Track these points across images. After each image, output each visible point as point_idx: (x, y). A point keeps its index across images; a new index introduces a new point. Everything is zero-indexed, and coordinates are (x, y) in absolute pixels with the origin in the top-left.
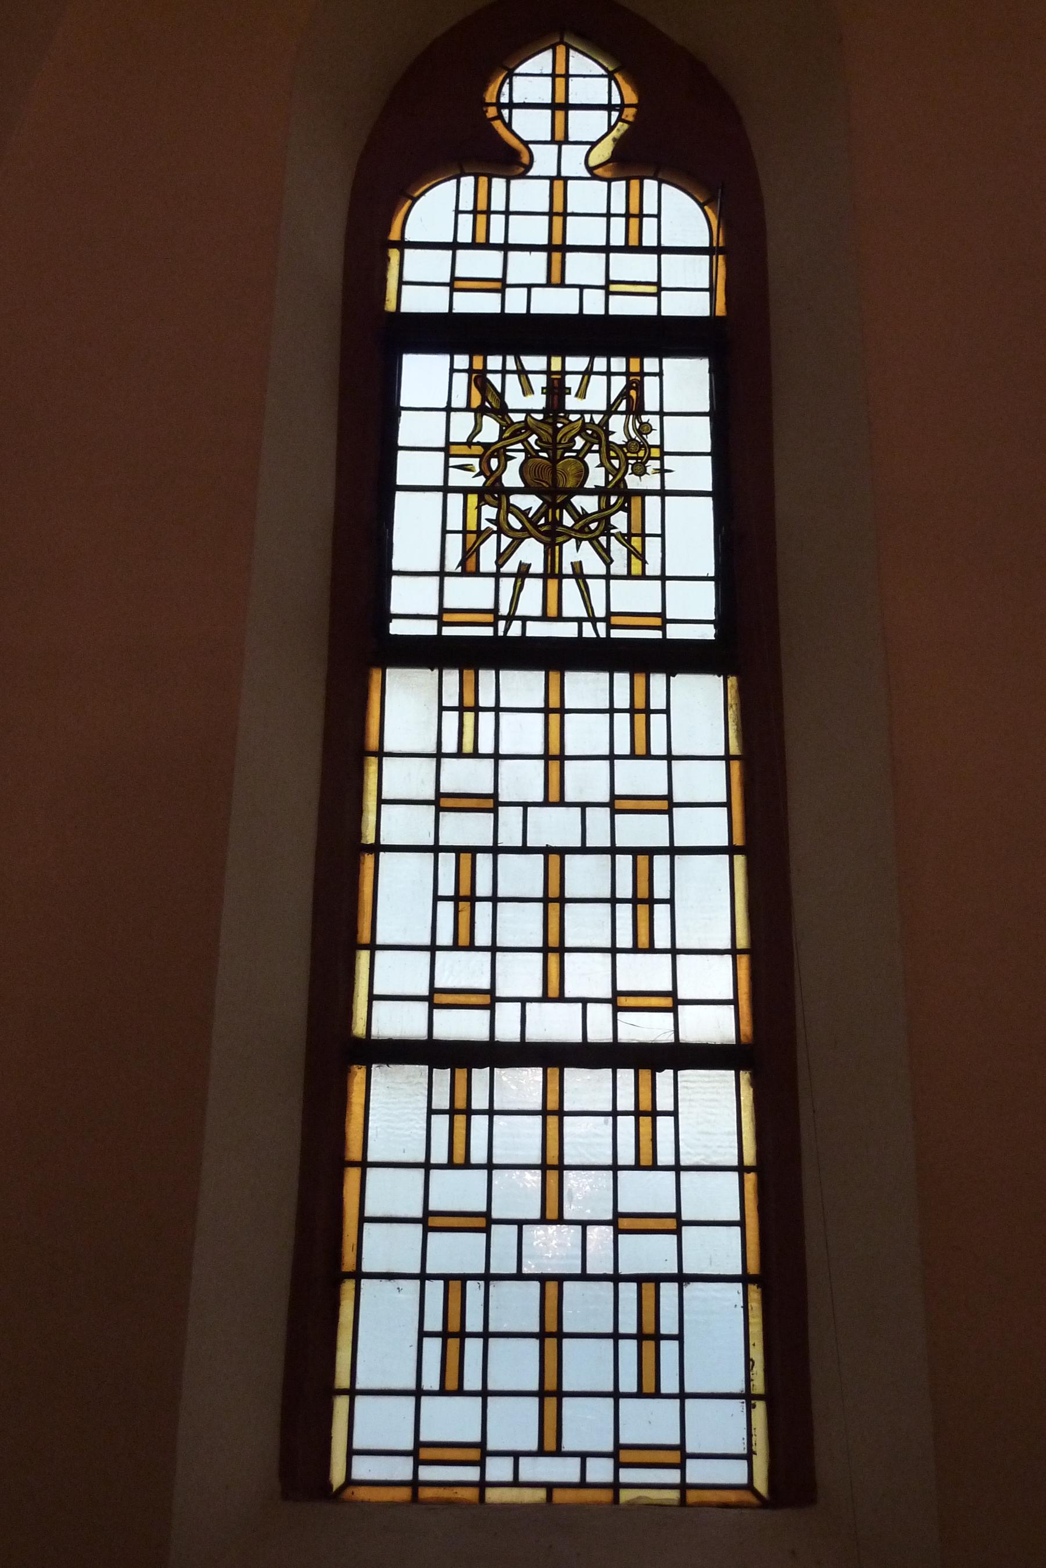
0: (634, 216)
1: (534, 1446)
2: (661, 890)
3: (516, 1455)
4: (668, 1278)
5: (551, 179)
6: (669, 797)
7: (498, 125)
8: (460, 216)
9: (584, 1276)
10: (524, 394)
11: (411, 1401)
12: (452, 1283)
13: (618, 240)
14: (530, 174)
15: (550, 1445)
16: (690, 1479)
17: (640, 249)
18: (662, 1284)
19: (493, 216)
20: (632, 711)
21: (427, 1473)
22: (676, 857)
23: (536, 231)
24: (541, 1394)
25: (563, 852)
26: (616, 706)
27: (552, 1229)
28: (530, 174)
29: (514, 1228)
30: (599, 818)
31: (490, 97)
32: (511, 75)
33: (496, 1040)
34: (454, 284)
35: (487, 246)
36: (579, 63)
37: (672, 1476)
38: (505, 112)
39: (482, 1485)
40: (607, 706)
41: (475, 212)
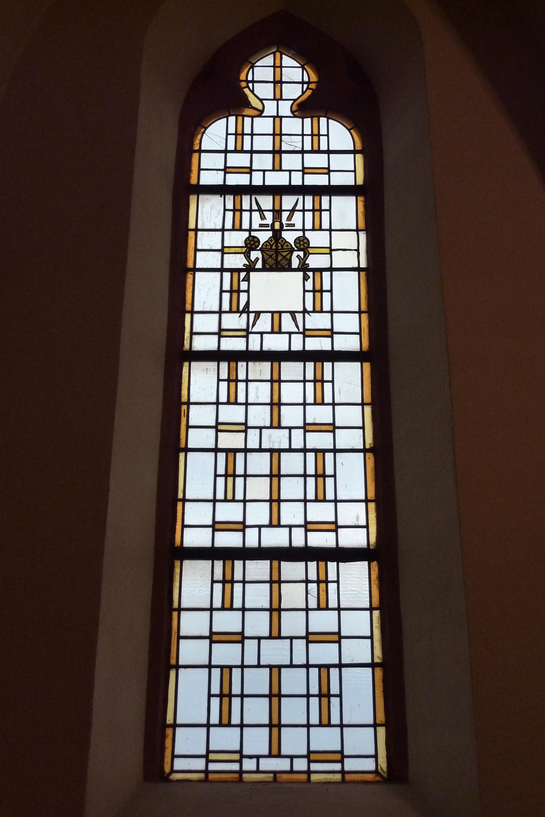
0: (316, 135)
1: (266, 752)
2: (329, 471)
3: (258, 757)
4: (334, 666)
5: (274, 117)
6: (335, 523)
7: (246, 91)
8: (229, 136)
9: (291, 666)
10: (260, 224)
11: (204, 730)
12: (224, 670)
13: (308, 147)
14: (263, 115)
15: (275, 751)
16: (347, 768)
17: (319, 152)
18: (326, 454)
19: (245, 137)
20: (315, 381)
21: (212, 767)
22: (337, 454)
23: (266, 143)
24: (270, 726)
25: (280, 451)
26: (307, 379)
27: (276, 447)
28: (263, 115)
29: (257, 529)
30: (297, 435)
31: (243, 77)
32: (253, 67)
33: (246, 547)
34: (226, 170)
35: (242, 151)
36: (287, 61)
37: (337, 767)
38: (250, 85)
39: (241, 772)
40: (305, 722)
41: (236, 134)
